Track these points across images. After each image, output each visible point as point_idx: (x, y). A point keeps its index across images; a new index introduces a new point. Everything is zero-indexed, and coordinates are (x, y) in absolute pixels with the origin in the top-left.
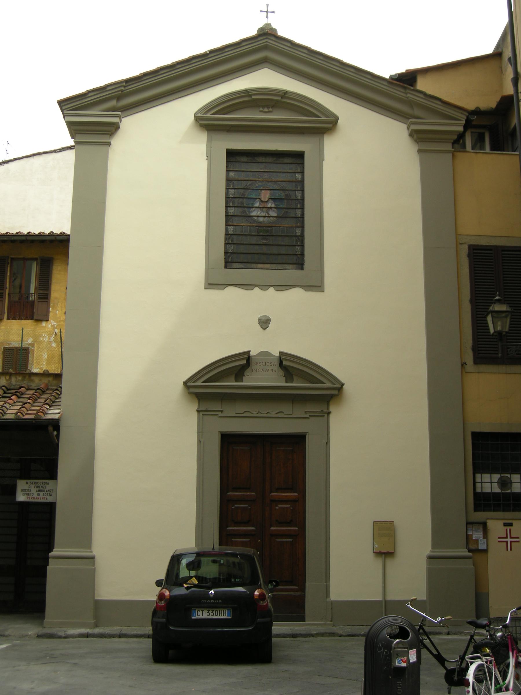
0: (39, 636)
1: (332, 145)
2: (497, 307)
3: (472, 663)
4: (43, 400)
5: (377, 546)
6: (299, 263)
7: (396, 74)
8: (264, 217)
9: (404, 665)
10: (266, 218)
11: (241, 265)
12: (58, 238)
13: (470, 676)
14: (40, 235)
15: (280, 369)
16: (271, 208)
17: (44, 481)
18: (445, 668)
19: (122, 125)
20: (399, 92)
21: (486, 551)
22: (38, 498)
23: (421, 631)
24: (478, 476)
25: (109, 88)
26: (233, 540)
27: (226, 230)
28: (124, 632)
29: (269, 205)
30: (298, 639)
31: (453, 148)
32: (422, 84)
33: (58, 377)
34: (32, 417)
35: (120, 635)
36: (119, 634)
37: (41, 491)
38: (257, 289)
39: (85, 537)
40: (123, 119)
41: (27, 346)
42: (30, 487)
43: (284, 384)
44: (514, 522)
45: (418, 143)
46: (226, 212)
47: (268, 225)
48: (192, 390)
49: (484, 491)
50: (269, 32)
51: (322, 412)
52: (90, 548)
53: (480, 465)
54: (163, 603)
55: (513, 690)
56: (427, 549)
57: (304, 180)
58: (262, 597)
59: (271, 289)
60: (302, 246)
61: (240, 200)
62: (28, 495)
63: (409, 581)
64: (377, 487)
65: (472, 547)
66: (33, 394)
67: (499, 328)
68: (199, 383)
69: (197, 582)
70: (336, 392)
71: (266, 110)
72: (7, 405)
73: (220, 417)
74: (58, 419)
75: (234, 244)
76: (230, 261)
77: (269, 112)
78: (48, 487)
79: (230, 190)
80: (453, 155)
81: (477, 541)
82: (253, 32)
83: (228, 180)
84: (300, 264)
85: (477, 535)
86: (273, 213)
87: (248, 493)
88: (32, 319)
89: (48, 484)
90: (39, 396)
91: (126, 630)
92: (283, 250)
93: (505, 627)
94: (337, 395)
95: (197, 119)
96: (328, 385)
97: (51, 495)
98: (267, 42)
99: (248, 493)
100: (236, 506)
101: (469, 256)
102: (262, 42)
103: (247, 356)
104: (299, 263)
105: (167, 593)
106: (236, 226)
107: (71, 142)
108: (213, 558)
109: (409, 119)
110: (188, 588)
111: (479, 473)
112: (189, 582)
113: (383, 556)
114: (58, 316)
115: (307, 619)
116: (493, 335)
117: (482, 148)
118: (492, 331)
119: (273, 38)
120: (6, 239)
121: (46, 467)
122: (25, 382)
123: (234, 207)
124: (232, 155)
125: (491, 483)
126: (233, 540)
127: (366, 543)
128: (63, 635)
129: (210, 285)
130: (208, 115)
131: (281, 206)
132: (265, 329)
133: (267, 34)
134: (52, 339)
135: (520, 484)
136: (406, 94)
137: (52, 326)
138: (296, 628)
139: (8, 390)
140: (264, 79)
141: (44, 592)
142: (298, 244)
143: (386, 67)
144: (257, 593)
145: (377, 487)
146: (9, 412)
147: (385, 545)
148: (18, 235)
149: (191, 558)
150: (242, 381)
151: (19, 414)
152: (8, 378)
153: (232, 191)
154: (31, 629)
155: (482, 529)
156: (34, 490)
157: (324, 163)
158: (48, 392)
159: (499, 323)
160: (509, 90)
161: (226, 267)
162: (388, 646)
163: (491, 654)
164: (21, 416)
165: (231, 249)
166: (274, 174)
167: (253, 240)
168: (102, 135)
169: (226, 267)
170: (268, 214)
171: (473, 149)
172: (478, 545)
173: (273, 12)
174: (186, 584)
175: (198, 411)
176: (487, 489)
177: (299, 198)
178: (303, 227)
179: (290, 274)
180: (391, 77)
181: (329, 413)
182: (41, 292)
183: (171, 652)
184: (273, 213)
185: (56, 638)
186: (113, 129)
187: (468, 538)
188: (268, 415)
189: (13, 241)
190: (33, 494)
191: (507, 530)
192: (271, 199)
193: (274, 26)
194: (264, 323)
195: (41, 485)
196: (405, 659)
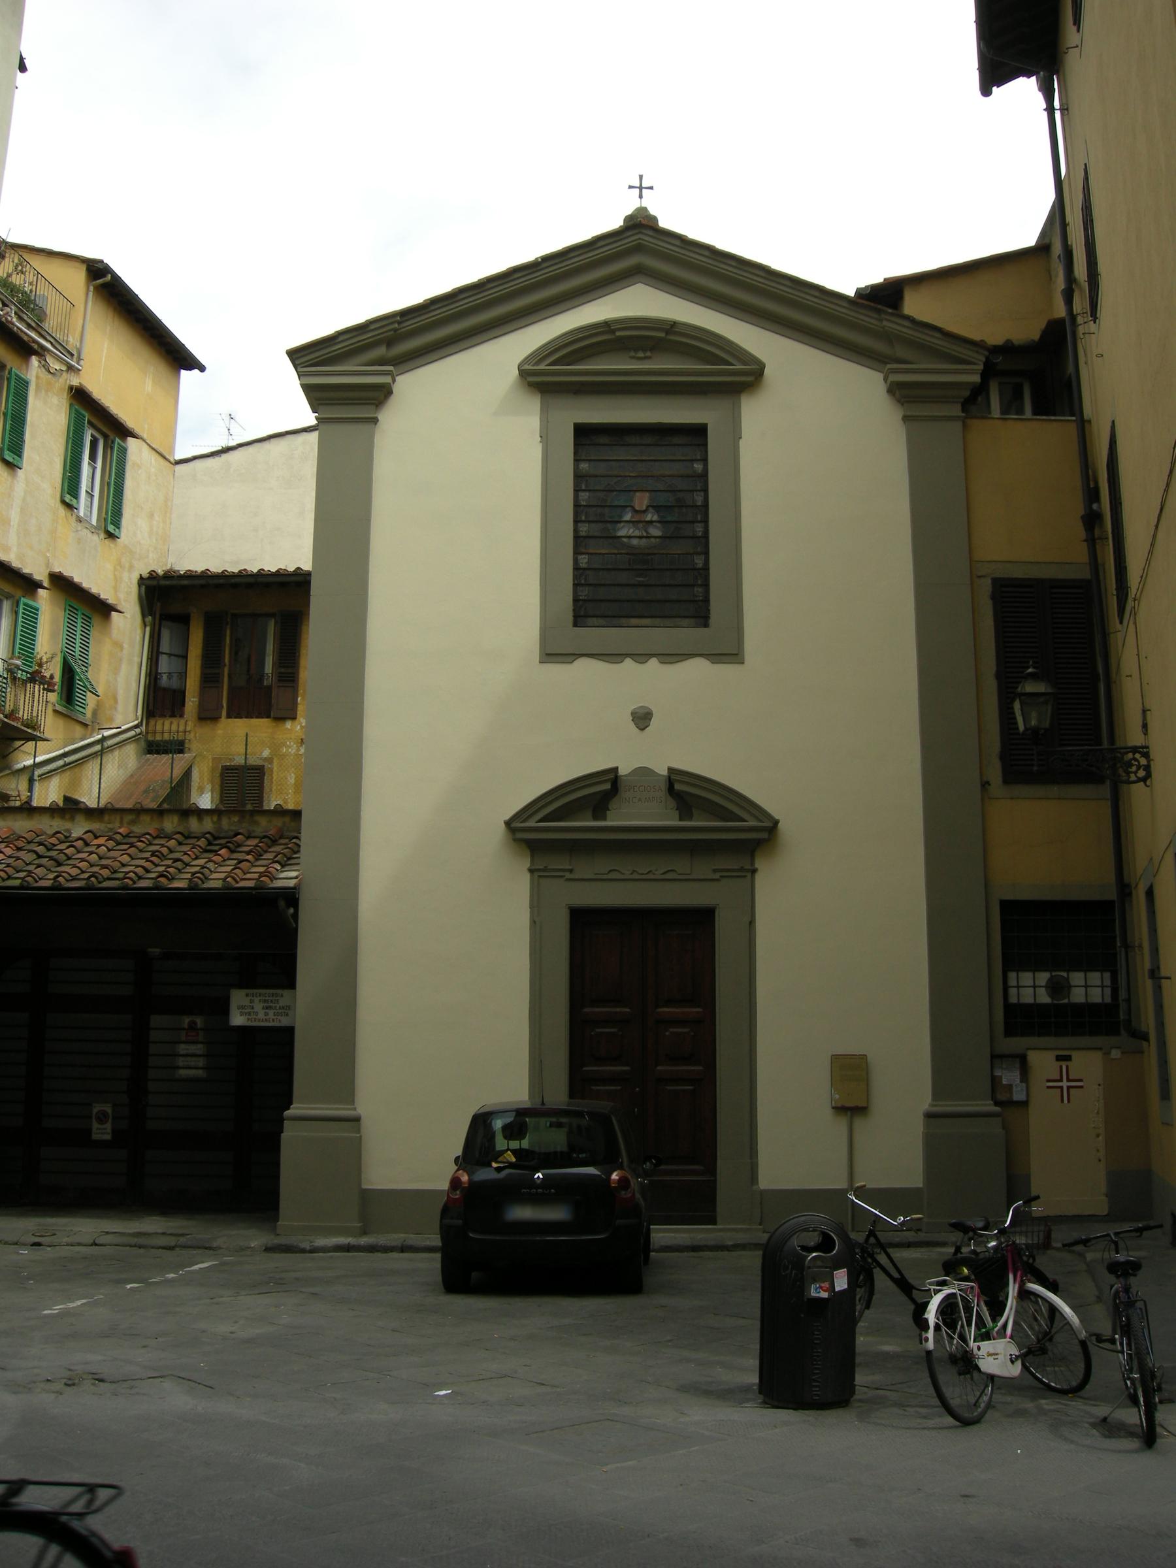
0: (268, 1249)
1: (755, 415)
2: (1030, 687)
3: (937, 1292)
4: (270, 856)
6: (700, 615)
7: (867, 287)
8: (640, 537)
9: (824, 1295)
10: (644, 540)
11: (601, 621)
13: (931, 1315)
14: (278, 573)
15: (669, 797)
16: (651, 522)
18: (913, 1300)
19: (395, 388)
20: (867, 319)
21: (1025, 1104)
23: (872, 1240)
24: (1012, 975)
25: (373, 327)
27: (576, 561)
28: (410, 1242)
29: (649, 518)
30: (701, 1254)
32: (914, 305)
33: (296, 814)
34: (251, 884)
38: (628, 662)
40: (398, 378)
41: (260, 763)
42: (252, 1001)
43: (676, 823)
44: (1074, 1054)
46: (576, 531)
47: (647, 551)
48: (519, 835)
49: (1022, 1001)
50: (643, 222)
51: (742, 869)
52: (353, 1102)
53: (1016, 955)
54: (457, 1195)
55: (1011, 1337)
56: (925, 1102)
58: (624, 1183)
59: (654, 662)
60: (706, 585)
61: (599, 510)
62: (249, 1014)
63: (895, 1152)
64: (839, 999)
65: (1001, 1097)
66: (257, 846)
67: (1033, 723)
68: (531, 823)
69: (514, 1160)
70: (765, 835)
71: (641, 354)
72: (211, 865)
74: (294, 888)
75: (590, 585)
76: (581, 616)
77: (646, 358)
79: (581, 494)
80: (965, 426)
83: (578, 476)
84: (702, 618)
85: (1009, 1076)
86: (655, 532)
87: (618, 1010)
88: (268, 717)
92: (35, 709)
93: (1003, 1231)
94: (768, 840)
95: (523, 373)
96: (752, 823)
99: (618, 1010)
101: (993, 597)
102: (631, 240)
103: (612, 776)
104: (700, 615)
105: (465, 1178)
107: (310, 419)
108: (554, 1120)
109: (887, 363)
110: (498, 1170)
112: (500, 1159)
115: (718, 1219)
116: (1023, 733)
117: (1020, 411)
118: (1021, 728)
119: (651, 233)
120: (222, 581)
122: (244, 825)
123: (589, 522)
124: (583, 433)
125: (1034, 987)
129: (550, 655)
130: (542, 367)
131: (669, 518)
132: (642, 729)
133: (640, 225)
138: (700, 1236)
141: (277, 1177)
143: (847, 276)
144: (615, 1176)
145: (839, 999)
146: (214, 876)
147: (852, 1091)
148: (243, 574)
149: (509, 1119)
150: (605, 819)
152: (215, 818)
153: (584, 496)
154: (256, 1238)
155: (1018, 1065)
156: (258, 1006)
157: (742, 443)
159: (1034, 714)
160: (1060, 311)
161: (575, 625)
162: (799, 1263)
163: (973, 1277)
164: (233, 883)
165: (584, 593)
166: (657, 464)
169: (575, 625)
171: (1002, 413)
173: (651, 188)
174: (497, 1162)
175: (531, 871)
176: (1027, 997)
177: (699, 503)
178: (706, 553)
180: (859, 292)
181: (754, 871)
182: (283, 670)
183: (474, 1275)
184: (655, 532)
186: (380, 395)
187: (995, 1081)
189: (235, 586)
193: (652, 212)
194: (642, 719)
196: (826, 1285)
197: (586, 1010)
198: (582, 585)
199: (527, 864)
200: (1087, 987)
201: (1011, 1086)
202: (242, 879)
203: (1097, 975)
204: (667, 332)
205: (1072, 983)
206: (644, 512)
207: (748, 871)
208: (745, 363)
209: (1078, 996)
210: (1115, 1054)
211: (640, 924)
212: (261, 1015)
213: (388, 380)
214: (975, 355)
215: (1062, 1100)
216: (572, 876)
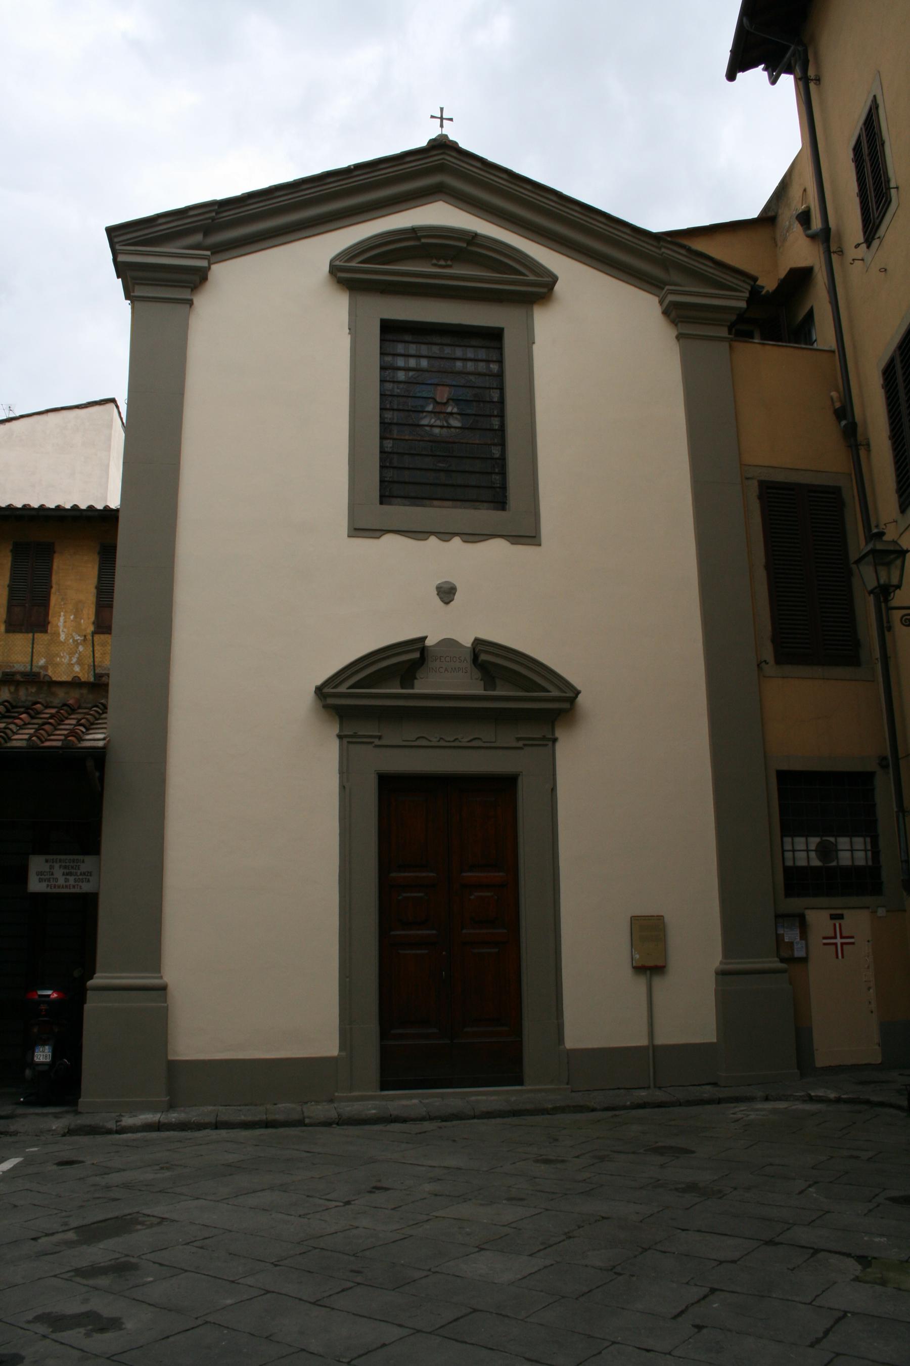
0: (71, 1132)
1: (547, 325)
5: (637, 956)
6: (498, 498)
8: (442, 427)
10: (445, 430)
12: (84, 513)
16: (451, 414)
19: (211, 276)
21: (804, 960)
24: (787, 840)
25: (192, 213)
26: (401, 952)
28: (224, 1118)
29: (449, 410)
31: (730, 333)
36: (214, 1121)
38: (433, 540)
39: (150, 950)
42: (51, 867)
43: (481, 692)
44: (845, 912)
45: (676, 325)
48: (331, 701)
51: (544, 738)
52: (159, 971)
56: (716, 959)
59: (457, 540)
60: (503, 473)
62: (49, 880)
63: (689, 1011)
68: (343, 689)
70: (566, 706)
71: (442, 263)
72: (12, 726)
73: (377, 746)
76: (388, 493)
78: (84, 868)
81: (791, 945)
82: (423, 143)
85: (791, 935)
86: (455, 422)
89: (83, 862)
90: (66, 715)
91: (227, 1114)
95: (334, 270)
96: (555, 693)
97: (89, 881)
100: (405, 895)
101: (760, 497)
102: (436, 158)
103: (420, 645)
104: (498, 498)
111: (802, 836)
113: (648, 972)
114: (83, 627)
119: (454, 154)
121: (81, 832)
122: (41, 696)
123: (393, 410)
126: (401, 952)
127: (619, 951)
128: (114, 1128)
129: (357, 530)
130: (353, 264)
131: (469, 411)
132: (447, 603)
134: (74, 660)
136: (660, 248)
137: (74, 641)
139: (14, 707)
150: (413, 688)
151: (34, 738)
152: (12, 689)
156: (58, 873)
157: (535, 347)
158: (80, 711)
161: (381, 503)
164: (39, 742)
168: (171, 306)
169: (381, 503)
170: (447, 422)
172: (793, 950)
175: (340, 737)
177: (496, 399)
179: (484, 516)
181: (555, 740)
184: (455, 422)
186: (197, 279)
187: (779, 939)
190: (57, 880)
191: (835, 925)
192: (453, 400)
194: (447, 593)
197: (393, 875)
198: (387, 467)
199: (336, 730)
200: (851, 852)
201: (792, 943)
202: (47, 740)
203: (860, 840)
204: (469, 243)
206: (445, 404)
207: (549, 739)
208: (537, 274)
209: (845, 859)
210: (881, 912)
211: (444, 787)
214: (742, 284)
215: (837, 957)
216: (383, 742)
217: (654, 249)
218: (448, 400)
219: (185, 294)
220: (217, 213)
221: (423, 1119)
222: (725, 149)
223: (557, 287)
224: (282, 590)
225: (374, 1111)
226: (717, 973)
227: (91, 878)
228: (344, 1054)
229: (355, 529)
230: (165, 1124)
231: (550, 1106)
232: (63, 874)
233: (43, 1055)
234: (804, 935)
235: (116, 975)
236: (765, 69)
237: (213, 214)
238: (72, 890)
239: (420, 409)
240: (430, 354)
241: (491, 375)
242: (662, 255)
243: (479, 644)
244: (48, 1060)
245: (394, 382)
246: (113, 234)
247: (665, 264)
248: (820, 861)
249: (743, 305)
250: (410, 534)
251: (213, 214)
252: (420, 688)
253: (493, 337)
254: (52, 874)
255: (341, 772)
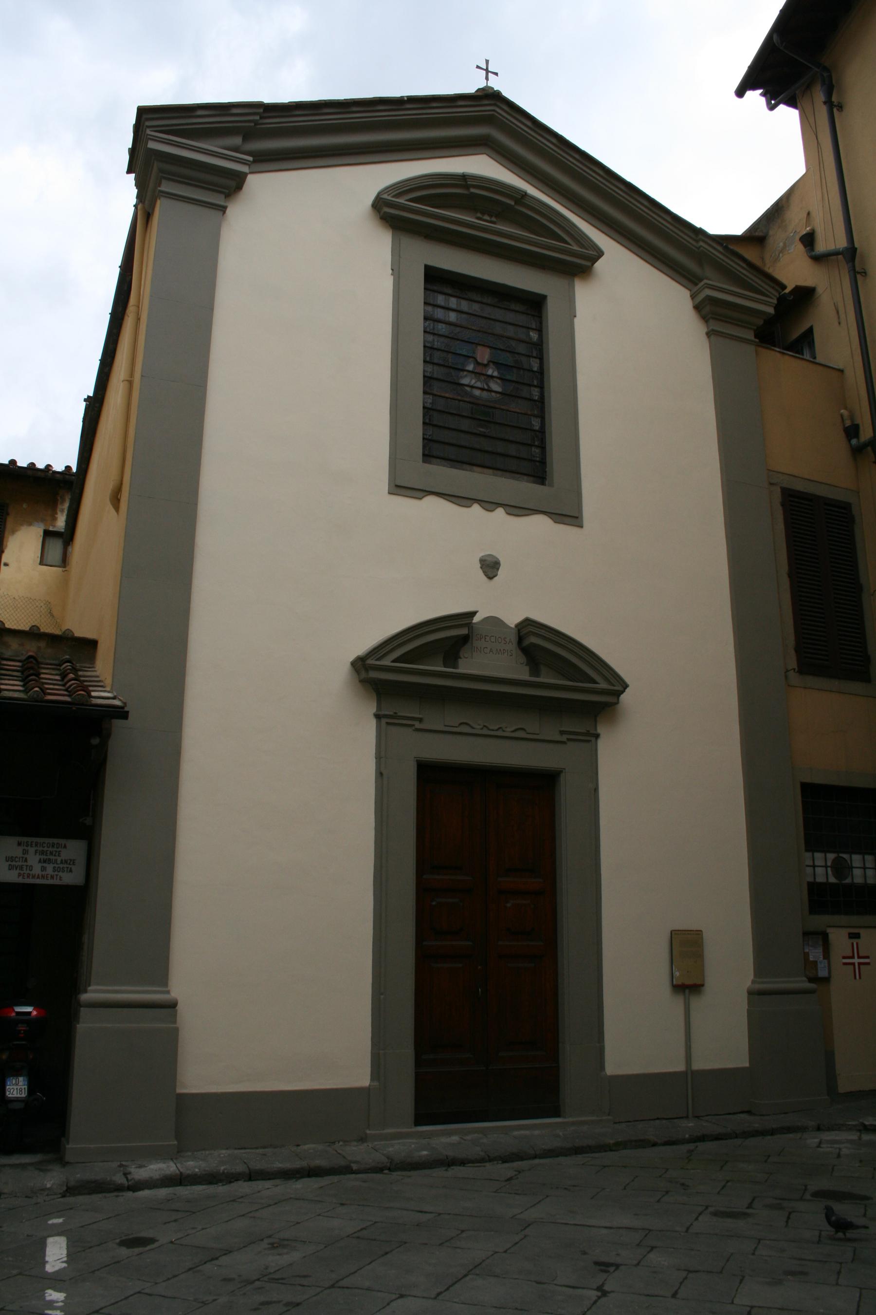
0: (70, 1190)
6: (538, 471)
8: (482, 389)
16: (492, 377)
17: (56, 841)
21: (826, 980)
22: (43, 876)
25: (235, 111)
29: (490, 372)
31: (756, 337)
35: (250, 1174)
37: (49, 861)
38: (476, 507)
39: (155, 962)
42: (25, 852)
43: (523, 674)
44: (862, 932)
48: (374, 675)
57: (542, 341)
59: (500, 511)
62: (21, 868)
63: (722, 1036)
68: (387, 662)
71: (486, 217)
73: (418, 730)
78: (65, 854)
81: (815, 963)
85: (816, 954)
89: (65, 847)
91: (256, 1159)
92: (512, 450)
96: (603, 685)
97: (71, 871)
98: (494, 111)
101: (783, 505)
102: (487, 108)
104: (538, 471)
106: (436, 395)
111: (859, 853)
113: (687, 991)
123: (434, 364)
124: (434, 278)
130: (401, 200)
131: (508, 377)
132: (491, 578)
135: (864, 870)
136: (697, 241)
140: (480, 165)
142: (536, 443)
150: (456, 667)
155: (821, 943)
156: (33, 859)
157: (576, 321)
167: (465, 424)
170: (487, 385)
172: (817, 970)
175: (378, 716)
177: (535, 369)
181: (597, 736)
184: (496, 387)
185: (110, 1191)
186: (230, 185)
187: (806, 955)
188: (499, 733)
190: (31, 868)
191: (853, 944)
194: (490, 567)
195: (50, 849)
205: (854, 865)
206: (486, 366)
208: (582, 246)
209: (857, 876)
212: (37, 870)
213: (244, 169)
217: (691, 241)
218: (489, 362)
219: (219, 200)
220: (261, 118)
221: (482, 1160)
222: (731, 164)
223: (599, 265)
224: (318, 548)
225: (425, 1153)
226: (750, 993)
227: (73, 868)
228: (376, 1084)
229: (397, 486)
230: (188, 1176)
231: (612, 1142)
232: (40, 861)
233: (17, 1088)
234: (827, 955)
235: (123, 988)
236: (762, 95)
237: (257, 118)
238: (50, 882)
239: (460, 367)
240: (470, 311)
241: (529, 342)
242: (698, 248)
243: (528, 627)
244: (23, 1095)
245: (434, 334)
246: (144, 116)
247: (701, 257)
248: (836, 878)
249: (771, 310)
250: (453, 499)
251: (257, 118)
252: (464, 667)
253: (535, 304)
254: (26, 860)
255: (379, 757)
